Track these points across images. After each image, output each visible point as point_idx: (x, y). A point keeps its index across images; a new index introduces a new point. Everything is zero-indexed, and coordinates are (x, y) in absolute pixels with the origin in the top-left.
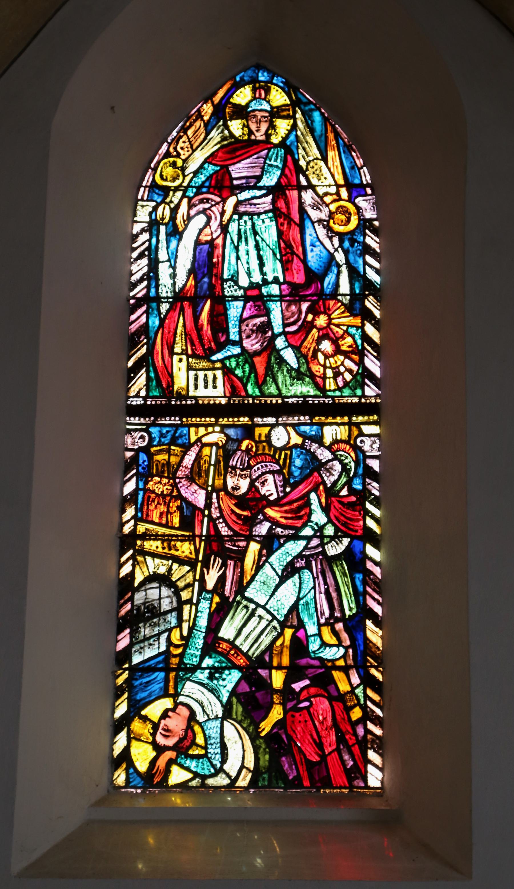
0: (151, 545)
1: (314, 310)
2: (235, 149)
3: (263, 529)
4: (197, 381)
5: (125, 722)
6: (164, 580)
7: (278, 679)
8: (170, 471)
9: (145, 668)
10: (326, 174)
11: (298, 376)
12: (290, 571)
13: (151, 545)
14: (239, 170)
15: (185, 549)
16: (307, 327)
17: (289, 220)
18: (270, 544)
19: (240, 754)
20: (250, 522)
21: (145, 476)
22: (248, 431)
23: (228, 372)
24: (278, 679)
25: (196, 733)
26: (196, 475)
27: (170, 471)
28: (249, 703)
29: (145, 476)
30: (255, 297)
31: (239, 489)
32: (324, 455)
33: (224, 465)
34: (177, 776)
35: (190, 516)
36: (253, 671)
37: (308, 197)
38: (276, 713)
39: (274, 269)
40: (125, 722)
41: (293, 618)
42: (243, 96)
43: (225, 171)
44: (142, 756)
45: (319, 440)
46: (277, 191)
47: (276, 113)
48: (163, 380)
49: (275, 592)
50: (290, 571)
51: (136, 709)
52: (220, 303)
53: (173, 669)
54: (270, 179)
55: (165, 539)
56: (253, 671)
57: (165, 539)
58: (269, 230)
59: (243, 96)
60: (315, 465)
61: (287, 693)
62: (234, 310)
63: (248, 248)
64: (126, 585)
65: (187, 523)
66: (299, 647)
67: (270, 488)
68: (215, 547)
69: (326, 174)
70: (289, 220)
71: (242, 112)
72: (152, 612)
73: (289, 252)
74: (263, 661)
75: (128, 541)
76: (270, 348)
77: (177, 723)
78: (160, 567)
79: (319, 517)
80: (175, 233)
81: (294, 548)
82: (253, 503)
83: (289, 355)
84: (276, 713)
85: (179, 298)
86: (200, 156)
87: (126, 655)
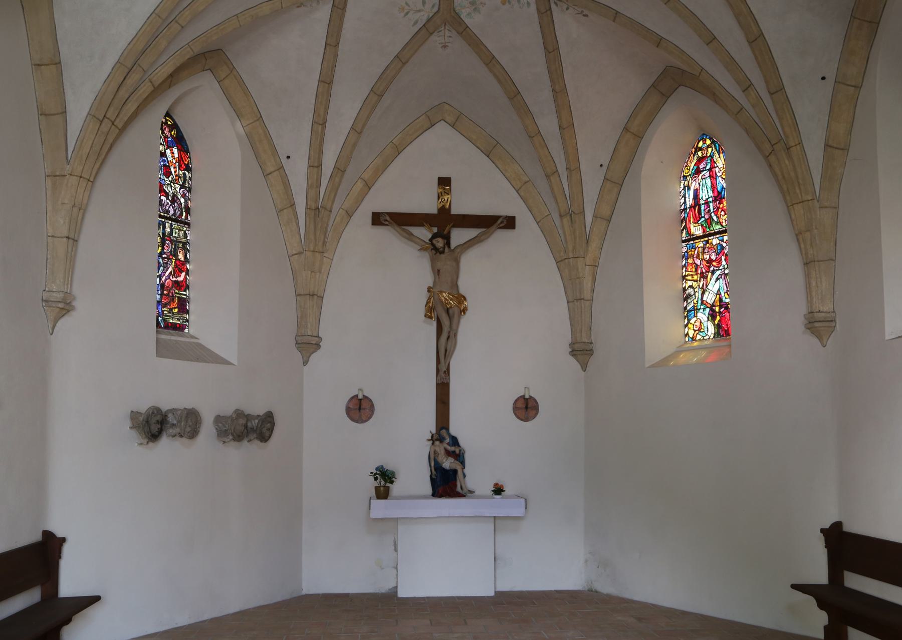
0: (689, 278)
1: (720, 203)
2: (700, 160)
3: (711, 269)
4: (697, 230)
5: (686, 326)
6: (691, 287)
7: (717, 309)
8: (692, 256)
9: (689, 311)
10: (720, 162)
11: (717, 223)
12: (718, 279)
13: (689, 278)
14: (701, 166)
15: (695, 278)
16: (718, 208)
17: (713, 177)
18: (713, 272)
19: (711, 330)
20: (709, 267)
21: (687, 259)
22: (707, 242)
23: (702, 226)
24: (717, 309)
25: (383, 587)
26: (698, 257)
27: (692, 256)
28: (712, 316)
29: (687, 259)
30: (707, 203)
31: (188, 287)
32: (724, 245)
33: (703, 253)
34: (699, 337)
35: (697, 267)
36: (712, 307)
37: (717, 169)
38: (718, 318)
39: (711, 194)
40: (686, 326)
41: (718, 293)
42: (701, 144)
43: (698, 168)
44: (691, 333)
45: (723, 241)
46: (710, 170)
47: (708, 147)
48: (689, 233)
49: (715, 286)
50: (718, 279)
51: (689, 320)
52: (700, 206)
53: (695, 309)
54: (708, 167)
55: (692, 275)
56: (712, 307)
57: (692, 275)
58: (708, 181)
59: (701, 144)
60: (723, 248)
61: (720, 313)
62: (703, 207)
63: (705, 188)
64: (684, 290)
65: (696, 270)
66: (721, 300)
67: (713, 257)
68: (703, 276)
69: (720, 162)
70: (713, 177)
71: (701, 149)
72: (689, 296)
73: (714, 187)
74: (713, 305)
75: (684, 277)
76: (711, 217)
77: (698, 324)
78: (690, 283)
79: (724, 263)
80: (689, 189)
81: (718, 273)
82: (710, 261)
83: (715, 218)
84: (718, 318)
85: (691, 207)
86: (693, 164)
87: (686, 308)
